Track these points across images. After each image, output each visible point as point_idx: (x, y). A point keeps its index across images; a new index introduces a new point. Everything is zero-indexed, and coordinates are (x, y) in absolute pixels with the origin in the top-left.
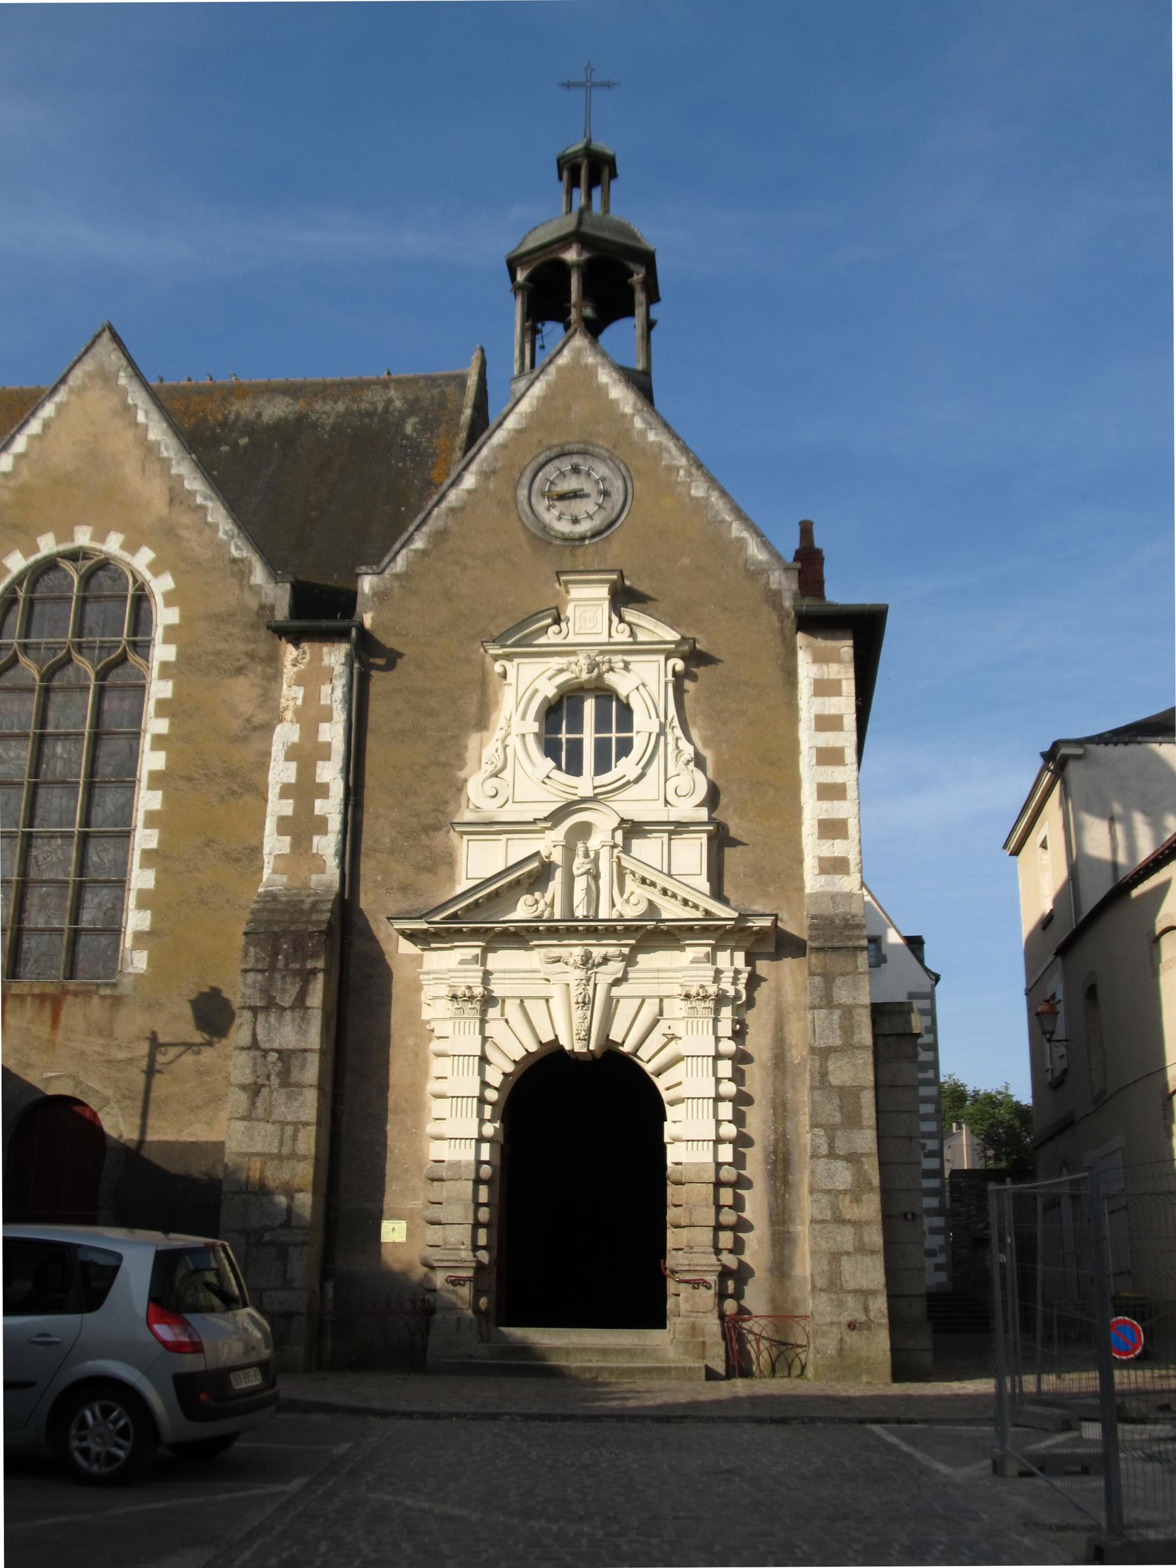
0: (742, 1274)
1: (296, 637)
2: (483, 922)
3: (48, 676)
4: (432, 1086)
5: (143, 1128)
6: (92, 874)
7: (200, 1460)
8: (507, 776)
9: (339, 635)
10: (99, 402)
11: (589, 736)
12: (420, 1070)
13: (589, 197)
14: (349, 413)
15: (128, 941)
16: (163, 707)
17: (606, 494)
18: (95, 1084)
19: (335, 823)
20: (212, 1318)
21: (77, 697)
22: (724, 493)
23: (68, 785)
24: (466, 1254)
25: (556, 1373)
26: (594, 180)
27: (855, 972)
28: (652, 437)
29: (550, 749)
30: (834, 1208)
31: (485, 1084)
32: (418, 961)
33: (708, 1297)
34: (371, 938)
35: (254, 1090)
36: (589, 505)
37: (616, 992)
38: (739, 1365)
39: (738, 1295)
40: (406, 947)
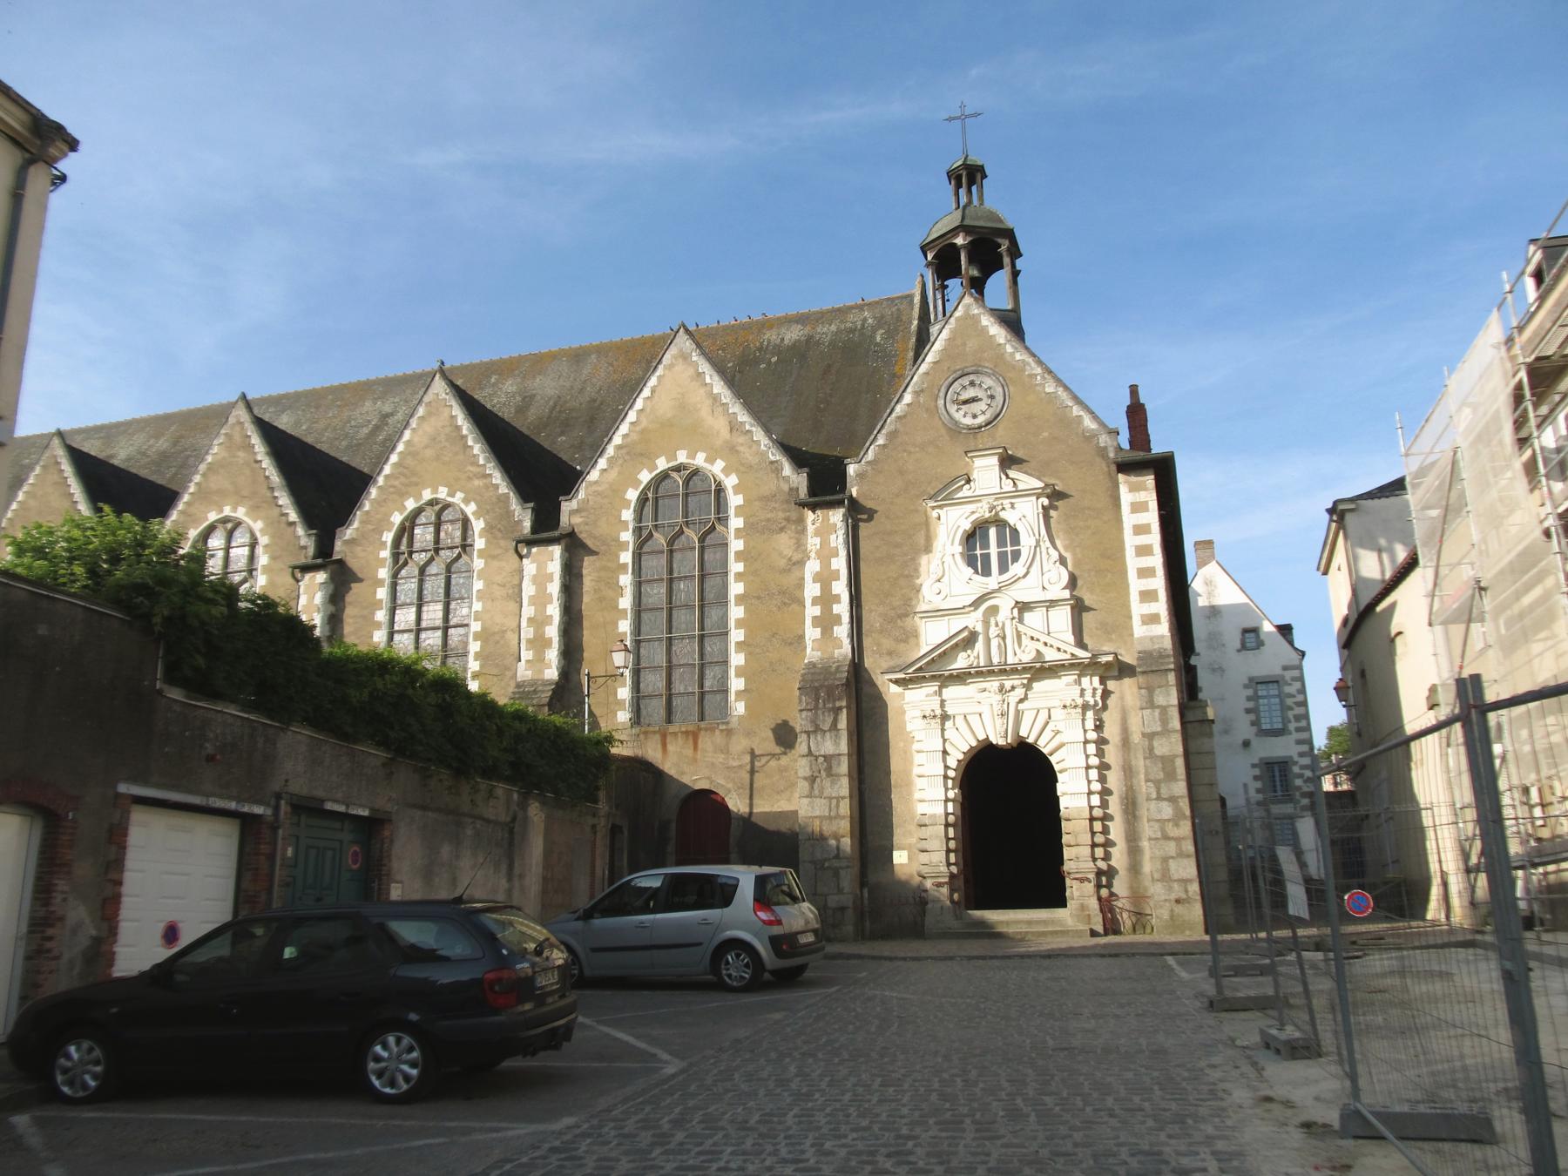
0: (1110, 873)
1: (814, 507)
2: (936, 670)
3: (671, 543)
4: (916, 771)
5: (751, 806)
6: (708, 659)
7: (788, 978)
8: (945, 581)
9: (840, 503)
10: (682, 372)
11: (993, 550)
12: (908, 760)
13: (969, 191)
14: (839, 331)
15: (732, 697)
16: (740, 556)
17: (992, 397)
18: (722, 782)
19: (846, 618)
20: (787, 908)
21: (689, 553)
22: (1066, 388)
23: (689, 607)
24: (943, 869)
25: (1000, 936)
26: (971, 182)
27: (1167, 685)
28: (1018, 357)
29: (971, 561)
30: (1163, 830)
31: (947, 767)
32: (902, 696)
33: (1090, 888)
34: (874, 685)
35: (812, 780)
36: (982, 406)
37: (1021, 706)
38: (1112, 927)
39: (1109, 886)
40: (894, 688)
